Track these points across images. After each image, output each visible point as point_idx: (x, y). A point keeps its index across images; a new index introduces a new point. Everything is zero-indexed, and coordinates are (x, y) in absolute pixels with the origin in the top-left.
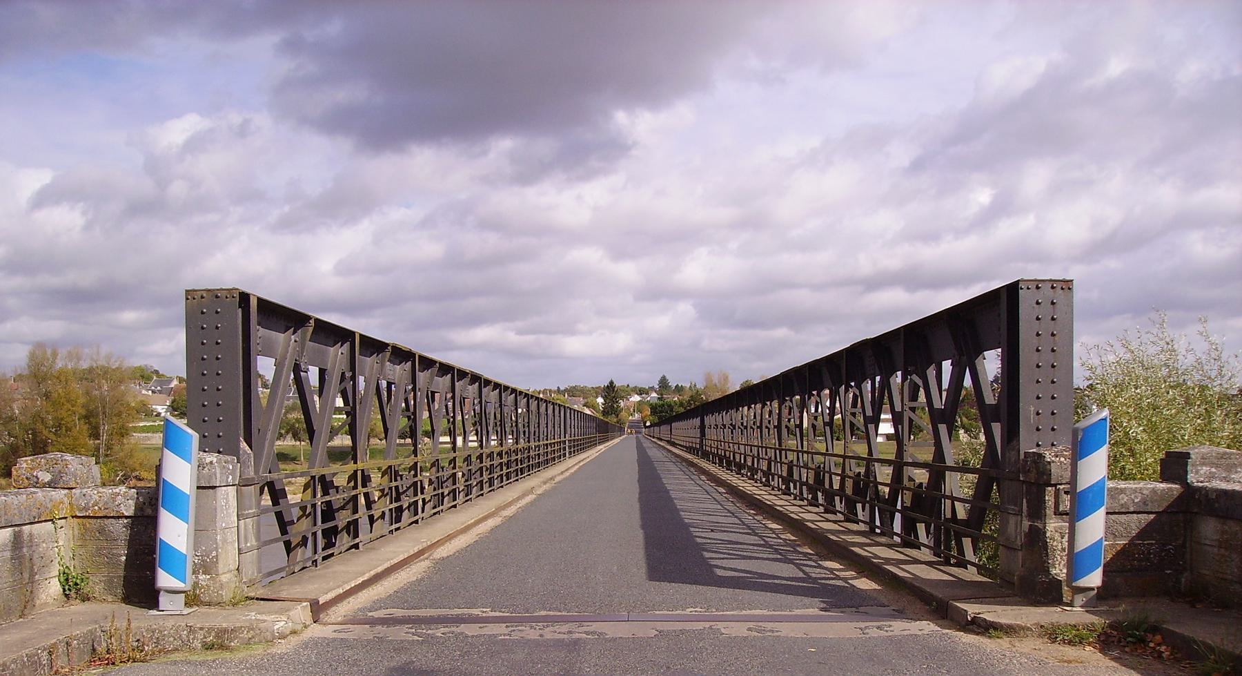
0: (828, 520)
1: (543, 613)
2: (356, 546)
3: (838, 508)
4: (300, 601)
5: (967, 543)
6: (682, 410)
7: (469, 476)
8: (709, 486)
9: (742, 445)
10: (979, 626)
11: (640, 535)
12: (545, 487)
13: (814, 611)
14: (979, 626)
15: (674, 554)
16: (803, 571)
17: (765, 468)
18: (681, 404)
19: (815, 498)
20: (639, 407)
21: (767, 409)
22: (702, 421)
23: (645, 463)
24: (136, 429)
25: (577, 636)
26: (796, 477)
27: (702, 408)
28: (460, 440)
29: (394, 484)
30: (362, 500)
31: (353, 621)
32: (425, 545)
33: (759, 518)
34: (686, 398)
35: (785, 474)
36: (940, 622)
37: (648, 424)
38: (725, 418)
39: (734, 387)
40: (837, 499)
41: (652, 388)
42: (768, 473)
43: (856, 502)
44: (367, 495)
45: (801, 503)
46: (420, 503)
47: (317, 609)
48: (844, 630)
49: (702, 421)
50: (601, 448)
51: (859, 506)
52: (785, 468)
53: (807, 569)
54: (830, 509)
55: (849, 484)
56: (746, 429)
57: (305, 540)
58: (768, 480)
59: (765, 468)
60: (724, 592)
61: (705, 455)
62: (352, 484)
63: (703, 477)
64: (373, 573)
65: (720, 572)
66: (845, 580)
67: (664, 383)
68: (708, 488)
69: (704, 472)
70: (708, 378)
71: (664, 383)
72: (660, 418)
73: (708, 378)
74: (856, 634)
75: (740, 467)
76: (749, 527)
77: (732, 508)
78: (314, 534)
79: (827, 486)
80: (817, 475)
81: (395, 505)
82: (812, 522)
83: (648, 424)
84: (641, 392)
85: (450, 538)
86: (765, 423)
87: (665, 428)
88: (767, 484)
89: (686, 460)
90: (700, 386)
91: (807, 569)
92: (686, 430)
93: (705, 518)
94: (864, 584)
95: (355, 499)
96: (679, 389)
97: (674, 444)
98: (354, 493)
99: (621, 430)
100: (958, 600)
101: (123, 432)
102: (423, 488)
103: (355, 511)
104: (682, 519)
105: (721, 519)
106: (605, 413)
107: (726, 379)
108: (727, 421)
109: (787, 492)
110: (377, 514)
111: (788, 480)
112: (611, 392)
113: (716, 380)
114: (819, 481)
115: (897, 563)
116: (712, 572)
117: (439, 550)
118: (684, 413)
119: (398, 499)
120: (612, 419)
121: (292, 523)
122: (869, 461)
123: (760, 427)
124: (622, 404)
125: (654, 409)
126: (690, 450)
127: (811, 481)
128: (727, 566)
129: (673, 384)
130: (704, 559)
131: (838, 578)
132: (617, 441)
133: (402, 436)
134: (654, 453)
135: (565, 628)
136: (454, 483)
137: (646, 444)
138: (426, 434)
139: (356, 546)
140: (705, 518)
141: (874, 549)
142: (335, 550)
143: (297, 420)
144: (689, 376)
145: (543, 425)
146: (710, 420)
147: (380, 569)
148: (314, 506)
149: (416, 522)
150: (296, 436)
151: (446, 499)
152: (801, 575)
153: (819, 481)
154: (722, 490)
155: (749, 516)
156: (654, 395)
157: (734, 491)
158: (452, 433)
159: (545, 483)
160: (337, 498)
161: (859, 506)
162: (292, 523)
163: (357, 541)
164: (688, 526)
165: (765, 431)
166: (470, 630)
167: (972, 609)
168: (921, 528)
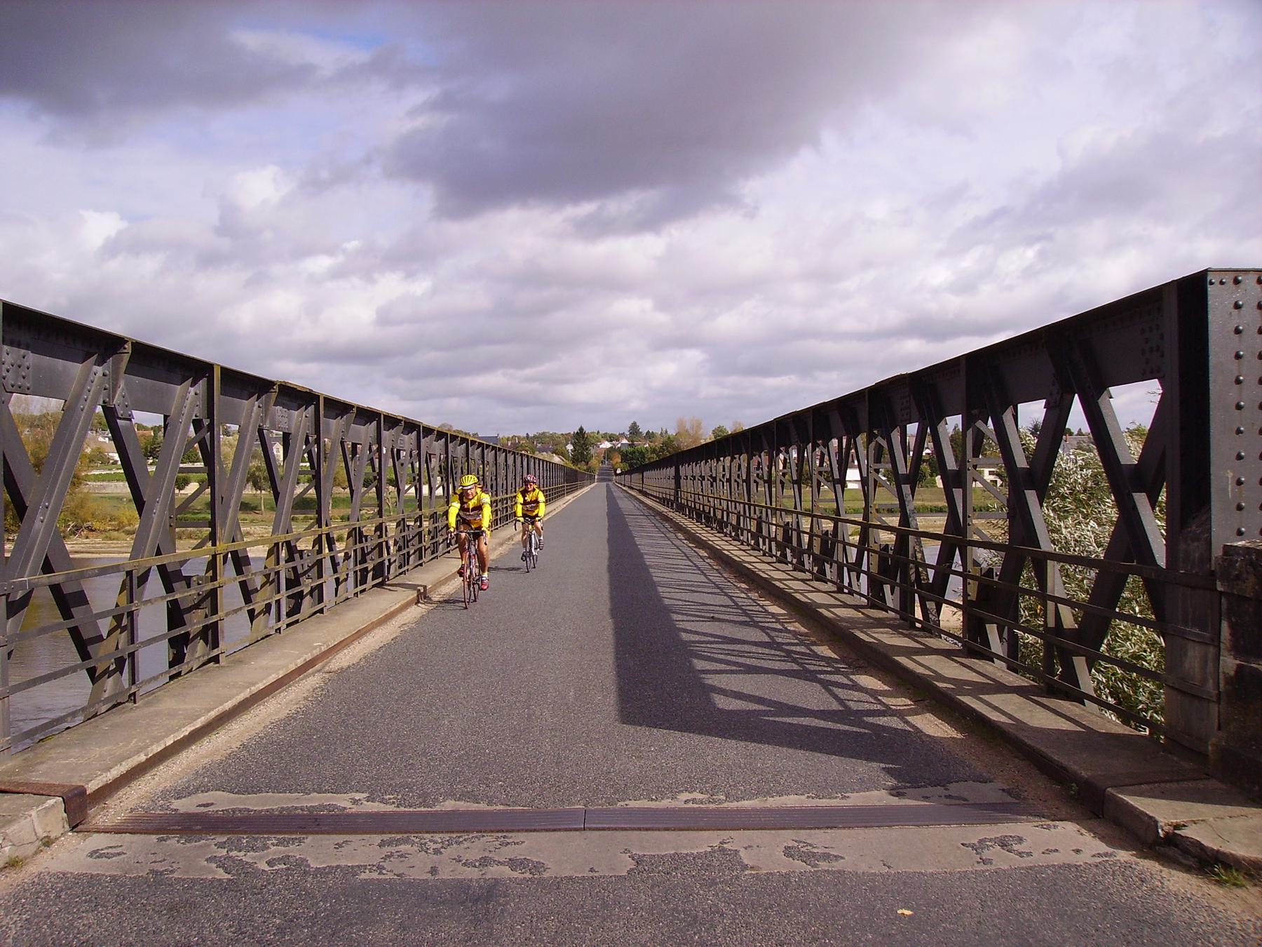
0: (846, 606)
1: (450, 805)
2: (216, 659)
3: (828, 577)
4: (43, 791)
5: (1080, 663)
6: (655, 457)
7: (402, 544)
8: (687, 546)
9: (720, 497)
10: (1186, 852)
11: (609, 623)
12: (501, 550)
13: (879, 797)
14: (1186, 852)
15: (656, 679)
16: (836, 697)
17: (754, 530)
18: (654, 451)
19: (822, 571)
20: (609, 453)
21: (736, 462)
22: (677, 471)
23: (616, 518)
24: (88, 478)
25: (494, 871)
26: (765, 533)
27: (678, 457)
28: (425, 489)
29: (359, 546)
30: (327, 564)
31: (139, 825)
32: (316, 652)
33: (754, 595)
34: (658, 444)
35: (754, 530)
36: (1094, 823)
37: (619, 471)
38: (702, 468)
39: (707, 437)
40: (806, 556)
41: (623, 435)
42: (737, 528)
43: (882, 584)
44: (333, 558)
45: (770, 559)
46: (387, 563)
47: (78, 806)
48: (939, 848)
49: (677, 471)
50: (569, 498)
51: (887, 588)
52: (754, 523)
53: (773, 634)
54: (799, 567)
55: (817, 542)
56: (711, 484)
57: (268, 606)
58: (757, 543)
59: (734, 523)
60: (732, 750)
61: (681, 508)
62: (317, 547)
63: (680, 536)
64: (213, 714)
65: (722, 702)
66: (900, 714)
67: (634, 430)
68: (687, 551)
69: (679, 528)
70: (681, 424)
71: (634, 430)
72: (631, 465)
73: (681, 424)
74: (966, 863)
75: (721, 526)
76: (745, 613)
77: (718, 580)
78: (278, 602)
79: (795, 543)
80: (786, 532)
81: (359, 567)
82: (780, 580)
83: (619, 471)
84: (611, 438)
85: (359, 634)
86: (734, 477)
87: (636, 476)
88: (736, 538)
89: (660, 514)
90: (672, 432)
91: (773, 634)
92: (659, 480)
93: (687, 596)
94: (932, 726)
95: (319, 563)
96: (650, 436)
97: (645, 494)
98: (319, 557)
99: (592, 479)
100: (1120, 786)
101: (77, 481)
102: (388, 548)
103: (320, 576)
104: (660, 599)
105: (679, 562)
106: (575, 460)
107: (699, 426)
108: (689, 474)
109: (756, 547)
110: (258, 606)
111: (757, 534)
112: (581, 438)
113: (688, 427)
114: (788, 538)
115: (909, 652)
116: (710, 701)
117: (341, 655)
118: (655, 461)
119: (363, 561)
120: (582, 467)
121: (256, 591)
122: (837, 518)
123: (729, 480)
124: (592, 451)
125: (625, 457)
126: (663, 501)
127: (780, 538)
128: (733, 688)
129: (643, 430)
130: (692, 669)
131: (888, 712)
132: (586, 489)
133: (367, 484)
134: (626, 505)
135: (475, 846)
136: (420, 542)
137: (617, 493)
138: (390, 482)
139: (216, 659)
140: (687, 596)
141: (758, 566)
142: (184, 668)
143: (258, 469)
144: (661, 423)
145: (510, 476)
146: (685, 470)
147: (228, 705)
148: (278, 573)
149: (321, 611)
150: (257, 486)
151: (370, 575)
152: (835, 706)
153: (788, 538)
154: (703, 553)
155: (741, 592)
156: (625, 441)
157: (717, 555)
158: (417, 482)
159: (501, 545)
160: (302, 564)
161: (887, 588)
162: (256, 591)
163: (215, 652)
164: (668, 610)
165: (734, 485)
166: (318, 852)
167: (1164, 812)
168: (992, 630)
